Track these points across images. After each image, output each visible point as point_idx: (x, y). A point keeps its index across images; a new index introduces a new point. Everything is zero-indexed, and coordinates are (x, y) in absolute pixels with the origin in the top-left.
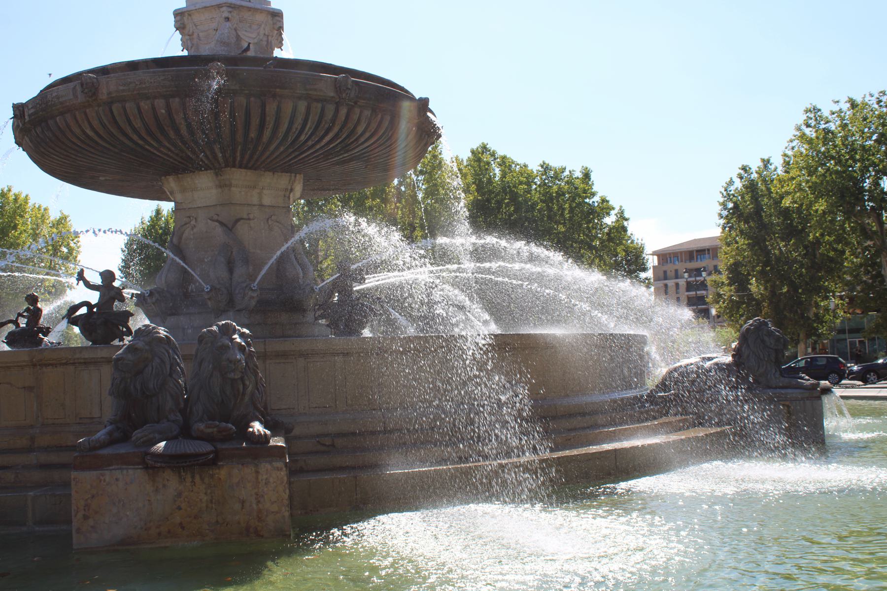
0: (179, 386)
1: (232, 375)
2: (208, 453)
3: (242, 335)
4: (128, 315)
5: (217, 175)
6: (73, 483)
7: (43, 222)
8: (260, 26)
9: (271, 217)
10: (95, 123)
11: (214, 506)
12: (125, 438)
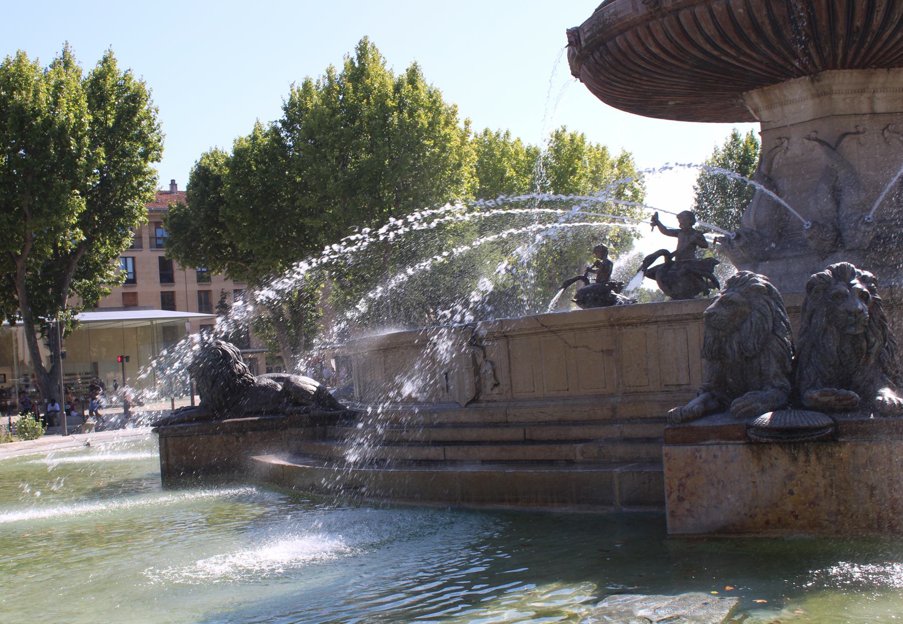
0: (784, 345)
1: (852, 330)
2: (825, 427)
3: (863, 279)
4: (712, 262)
5: (812, 81)
6: (665, 459)
7: (602, 162)
10: (661, 37)
11: (834, 491)
12: (722, 408)
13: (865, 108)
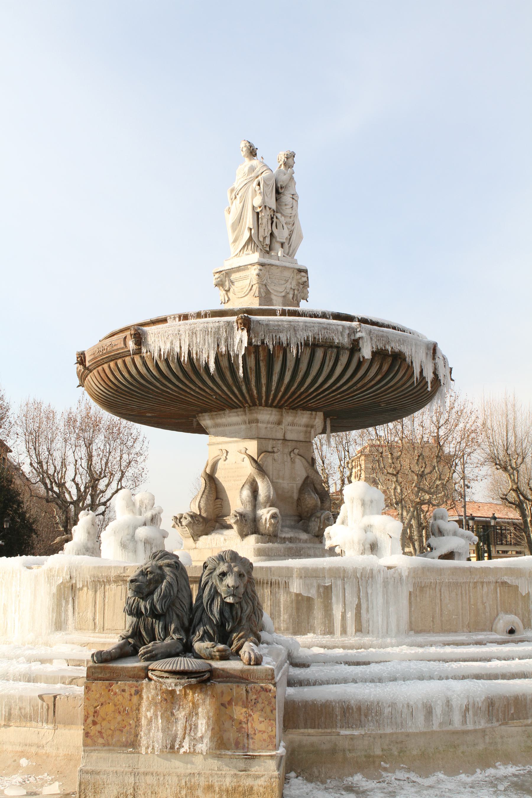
8: (287, 281)
9: (293, 450)
13: (280, 436)
